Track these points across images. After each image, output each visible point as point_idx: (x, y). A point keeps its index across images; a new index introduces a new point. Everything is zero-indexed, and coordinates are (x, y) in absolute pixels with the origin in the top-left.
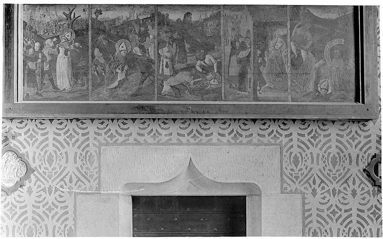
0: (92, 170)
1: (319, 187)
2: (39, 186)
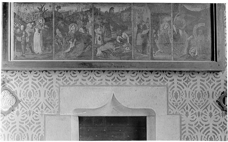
0: (55, 101)
1: (190, 111)
2: (23, 111)
